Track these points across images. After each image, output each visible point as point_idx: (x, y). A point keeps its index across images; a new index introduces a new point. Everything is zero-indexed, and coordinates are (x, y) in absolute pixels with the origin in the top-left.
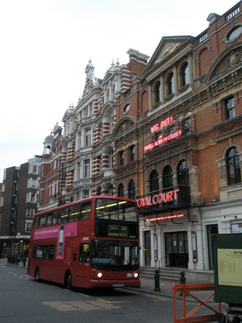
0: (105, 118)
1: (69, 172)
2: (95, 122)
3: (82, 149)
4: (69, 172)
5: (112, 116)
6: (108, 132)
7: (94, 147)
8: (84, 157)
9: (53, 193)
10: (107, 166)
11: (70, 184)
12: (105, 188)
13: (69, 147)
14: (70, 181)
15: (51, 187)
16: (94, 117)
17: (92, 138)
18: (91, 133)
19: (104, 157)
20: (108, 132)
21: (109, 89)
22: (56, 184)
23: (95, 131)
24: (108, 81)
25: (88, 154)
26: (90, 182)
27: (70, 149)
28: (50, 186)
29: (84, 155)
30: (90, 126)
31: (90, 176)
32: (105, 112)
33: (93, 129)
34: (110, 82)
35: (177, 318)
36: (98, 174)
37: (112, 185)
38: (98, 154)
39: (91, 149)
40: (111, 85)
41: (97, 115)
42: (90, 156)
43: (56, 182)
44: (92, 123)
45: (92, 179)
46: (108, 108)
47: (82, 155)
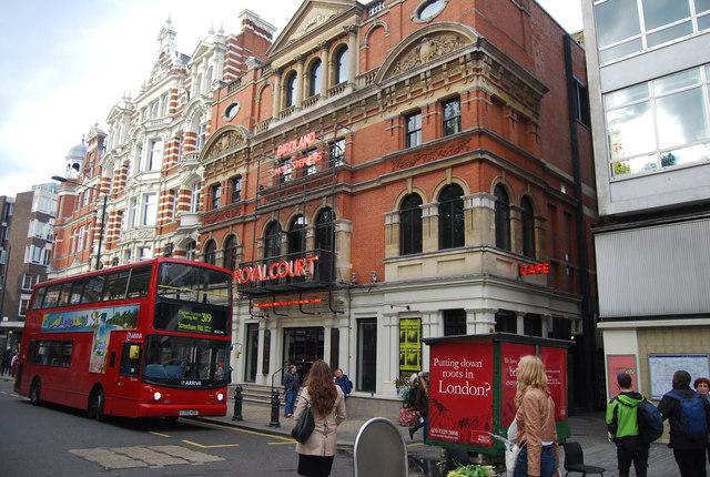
1: (113, 214)
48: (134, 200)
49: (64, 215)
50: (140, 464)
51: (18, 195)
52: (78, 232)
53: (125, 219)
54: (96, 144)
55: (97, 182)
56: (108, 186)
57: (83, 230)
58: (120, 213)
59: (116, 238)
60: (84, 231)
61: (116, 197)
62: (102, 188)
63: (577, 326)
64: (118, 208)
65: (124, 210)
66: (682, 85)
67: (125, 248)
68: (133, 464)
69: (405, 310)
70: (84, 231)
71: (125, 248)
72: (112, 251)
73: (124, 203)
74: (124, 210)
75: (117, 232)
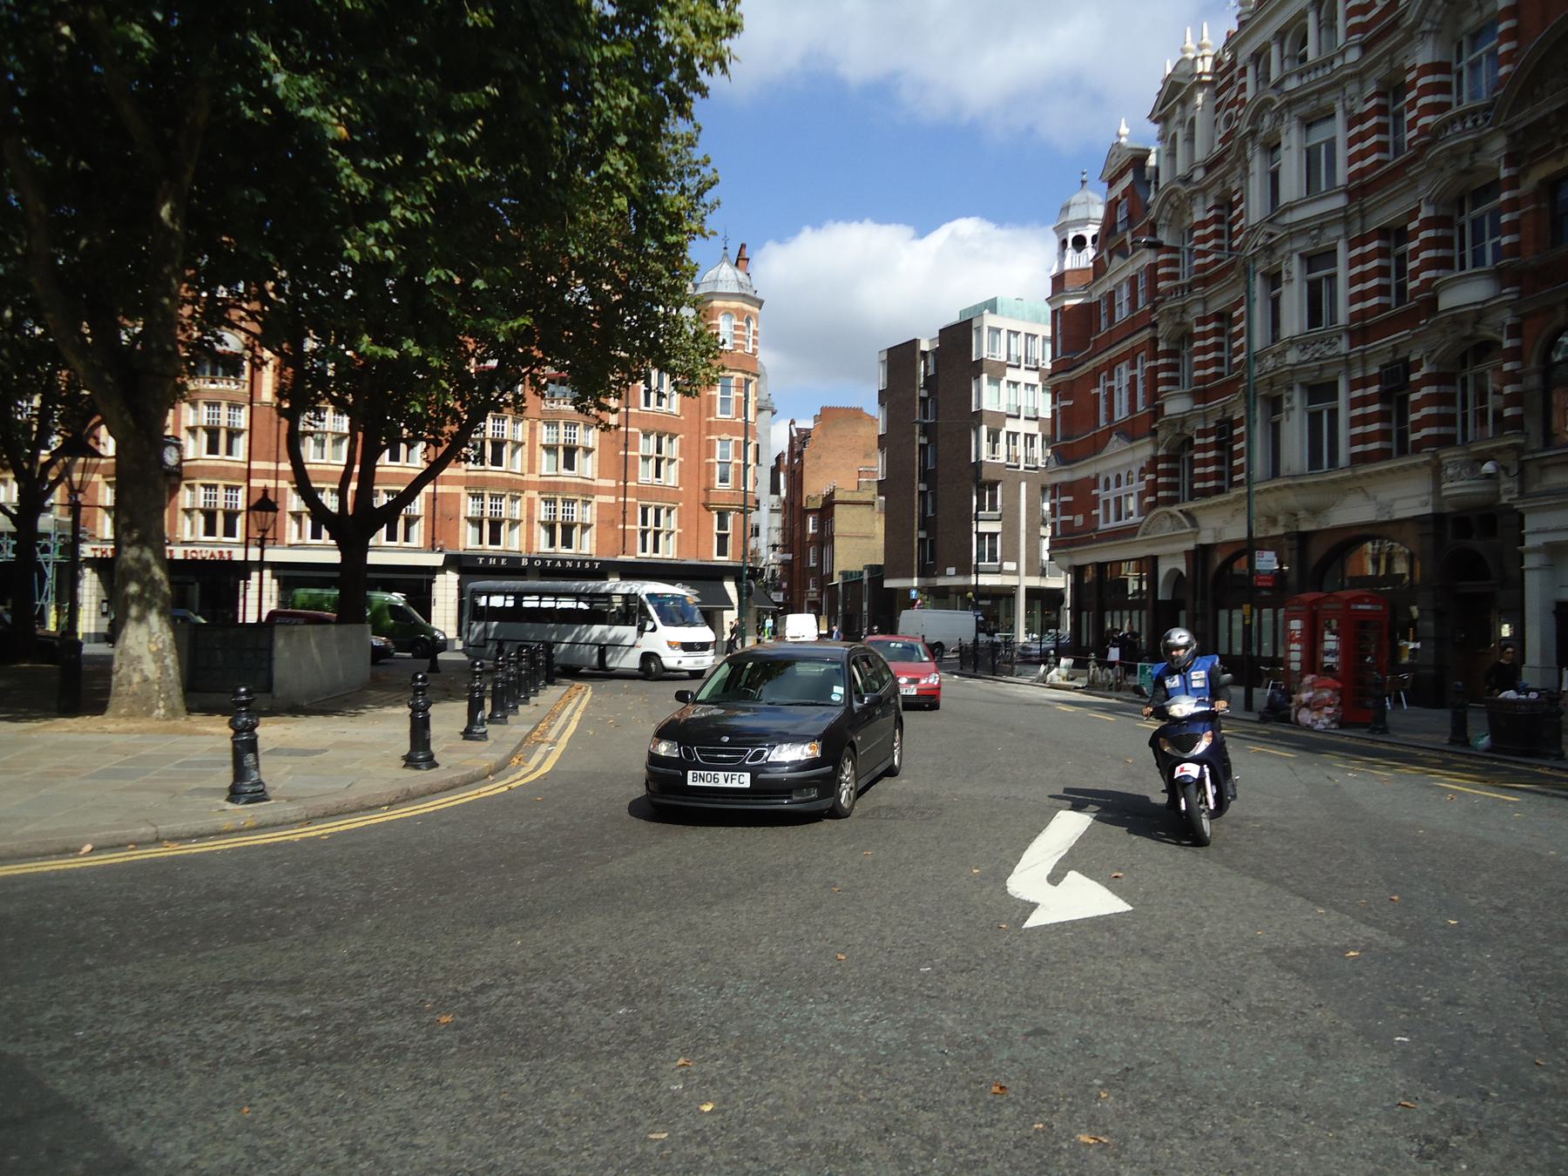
0: (1430, 41)
1: (1203, 321)
2: (1360, 75)
3: (1291, 207)
4: (1203, 321)
5: (1187, 222)
6: (1447, 106)
7: (1359, 190)
8: (1303, 244)
9: (1121, 413)
10: (1173, 381)
11: (1211, 371)
12: (1167, 448)
13: (1198, 216)
14: (1211, 355)
15: (1111, 389)
16: (1353, 55)
17: (1342, 154)
18: (1338, 129)
19: (1427, 224)
20: (1447, 106)
21: (1175, 136)
22: (1133, 379)
23: (1362, 118)
24: (1173, 109)
25: (1321, 227)
26: (1343, 346)
27: (1203, 224)
28: (1100, 390)
29: (1305, 231)
30: (1326, 99)
31: (1342, 319)
32: (1164, 214)
33: (1346, 112)
34: (1178, 109)
35: (821, 632)
36: (1217, 375)
37: (1191, 439)
38: (1384, 216)
39: (1340, 201)
40: (1181, 122)
41: (1365, 47)
42: (1335, 232)
43: (1134, 367)
44: (1339, 84)
45: (1351, 333)
46: (1174, 198)
47: (1291, 236)
52: (1111, 378)
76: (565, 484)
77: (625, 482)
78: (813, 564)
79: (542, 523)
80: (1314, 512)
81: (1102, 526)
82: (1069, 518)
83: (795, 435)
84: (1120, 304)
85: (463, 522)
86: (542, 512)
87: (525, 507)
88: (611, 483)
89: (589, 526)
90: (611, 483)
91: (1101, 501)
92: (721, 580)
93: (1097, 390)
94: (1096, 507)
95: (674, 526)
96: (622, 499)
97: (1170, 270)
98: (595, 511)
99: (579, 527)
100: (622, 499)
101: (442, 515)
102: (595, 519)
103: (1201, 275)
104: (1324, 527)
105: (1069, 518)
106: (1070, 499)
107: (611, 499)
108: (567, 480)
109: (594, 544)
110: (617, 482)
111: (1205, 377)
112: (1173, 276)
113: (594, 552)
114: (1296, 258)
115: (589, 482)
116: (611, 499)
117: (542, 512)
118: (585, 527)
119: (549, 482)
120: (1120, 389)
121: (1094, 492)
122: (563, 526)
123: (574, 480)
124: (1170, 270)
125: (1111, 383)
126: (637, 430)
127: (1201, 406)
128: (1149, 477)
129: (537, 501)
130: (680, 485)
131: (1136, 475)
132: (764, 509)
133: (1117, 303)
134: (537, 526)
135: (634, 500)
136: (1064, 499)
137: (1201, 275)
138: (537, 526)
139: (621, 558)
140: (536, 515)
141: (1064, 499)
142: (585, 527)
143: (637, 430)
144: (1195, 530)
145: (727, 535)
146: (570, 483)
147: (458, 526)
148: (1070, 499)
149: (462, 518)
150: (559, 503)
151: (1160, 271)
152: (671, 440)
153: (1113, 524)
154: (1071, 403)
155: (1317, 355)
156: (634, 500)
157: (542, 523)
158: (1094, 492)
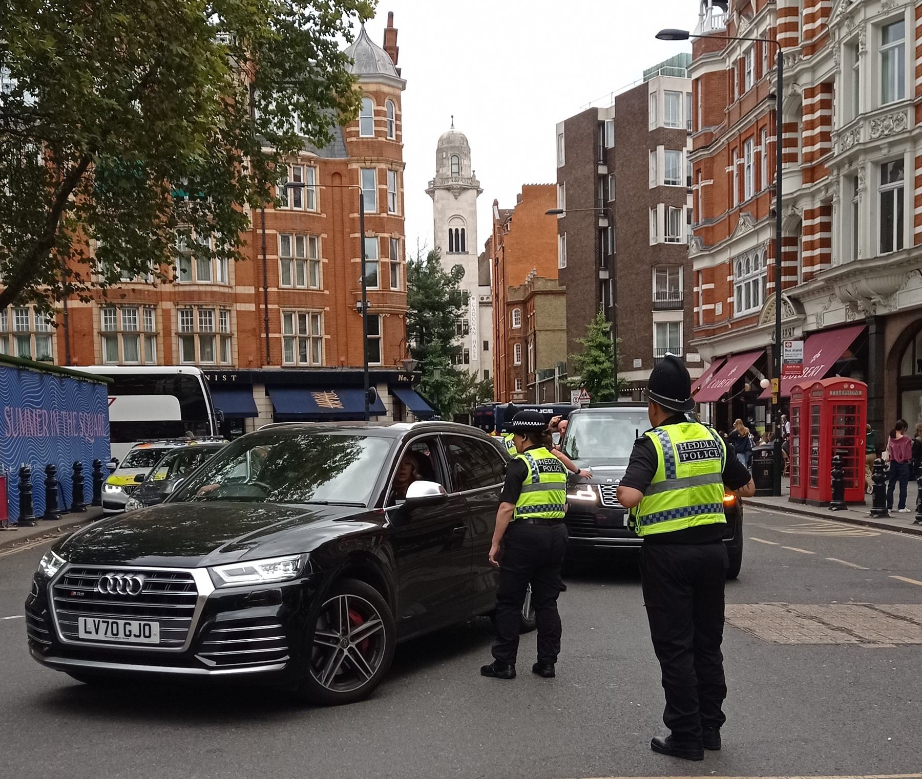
1: (811, 93)
15: (741, 167)
22: (758, 155)
43: (758, 143)
48: (854, 46)
49: (706, 123)
50: (842, 638)
51: (618, 99)
52: (741, 156)
53: (839, 101)
54: (603, 383)
55: (769, 22)
56: (793, 27)
57: (752, 149)
58: (827, 87)
59: (823, 151)
60: (753, 150)
61: (812, 49)
62: (779, 37)
63: (312, 274)
64: (822, 75)
65: (833, 78)
66: (372, 408)
67: (845, 170)
68: (831, 636)
69: (144, 281)
70: (753, 150)
71: (845, 170)
72: (820, 183)
73: (831, 64)
74: (833, 78)
75: (825, 137)
76: (200, 293)
77: (266, 288)
78: (517, 363)
79: (179, 335)
80: (888, 295)
81: (737, 315)
82: (711, 306)
83: (497, 217)
84: (749, 73)
85: (96, 339)
86: (178, 325)
87: (160, 319)
88: (251, 290)
89: (230, 336)
90: (251, 290)
91: (735, 287)
92: (249, 389)
93: (731, 168)
94: (731, 295)
95: (321, 332)
96: (262, 306)
97: (789, 35)
98: (235, 321)
99: (218, 338)
100: (262, 306)
101: (74, 331)
102: (235, 328)
103: (809, 42)
104: (894, 310)
105: (711, 306)
106: (711, 286)
107: (252, 307)
108: (202, 289)
109: (236, 355)
110: (257, 288)
111: (812, 153)
112: (793, 42)
113: (236, 363)
114: (869, 27)
115: (226, 290)
116: (252, 307)
117: (178, 325)
118: (225, 338)
119: (184, 292)
120: (749, 167)
121: (729, 278)
122: (201, 337)
123: (209, 289)
124: (789, 35)
125: (742, 160)
126: (274, 232)
127: (809, 185)
128: (770, 261)
129: (173, 312)
130: (326, 288)
131: (761, 260)
132: (473, 303)
133: (747, 71)
134: (174, 339)
135: (276, 306)
136: (705, 287)
137: (809, 42)
138: (174, 339)
139: (266, 368)
140: (173, 327)
141: (705, 287)
142: (225, 338)
143: (274, 232)
144: (802, 316)
145: (378, 339)
146: (206, 292)
147: (92, 342)
148: (711, 286)
149: (95, 333)
150: (196, 312)
151: (779, 37)
152: (312, 241)
153: (745, 312)
154: (711, 182)
155: (886, 132)
156: (276, 306)
157: (179, 335)
158: (729, 278)
